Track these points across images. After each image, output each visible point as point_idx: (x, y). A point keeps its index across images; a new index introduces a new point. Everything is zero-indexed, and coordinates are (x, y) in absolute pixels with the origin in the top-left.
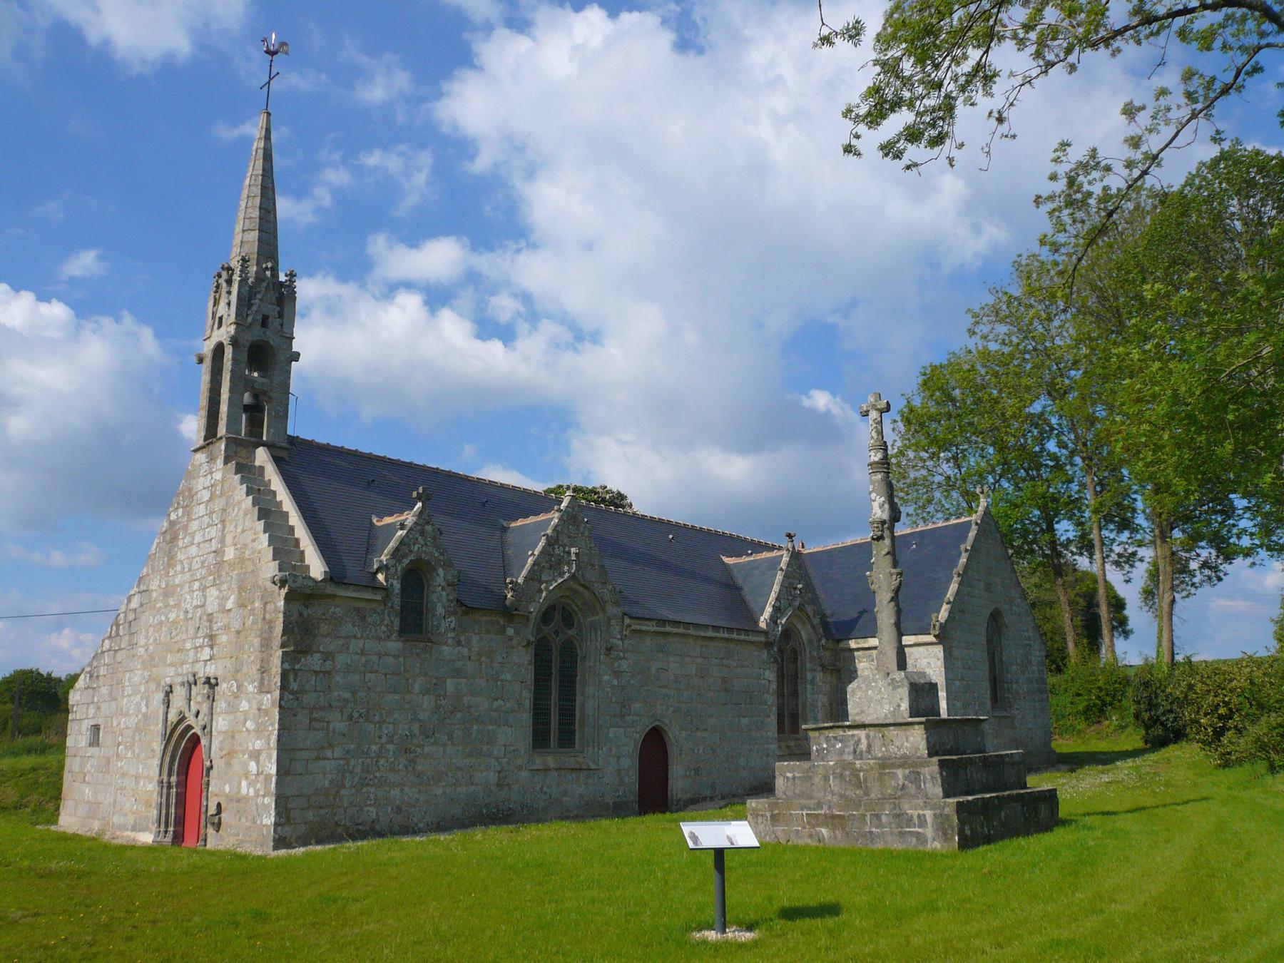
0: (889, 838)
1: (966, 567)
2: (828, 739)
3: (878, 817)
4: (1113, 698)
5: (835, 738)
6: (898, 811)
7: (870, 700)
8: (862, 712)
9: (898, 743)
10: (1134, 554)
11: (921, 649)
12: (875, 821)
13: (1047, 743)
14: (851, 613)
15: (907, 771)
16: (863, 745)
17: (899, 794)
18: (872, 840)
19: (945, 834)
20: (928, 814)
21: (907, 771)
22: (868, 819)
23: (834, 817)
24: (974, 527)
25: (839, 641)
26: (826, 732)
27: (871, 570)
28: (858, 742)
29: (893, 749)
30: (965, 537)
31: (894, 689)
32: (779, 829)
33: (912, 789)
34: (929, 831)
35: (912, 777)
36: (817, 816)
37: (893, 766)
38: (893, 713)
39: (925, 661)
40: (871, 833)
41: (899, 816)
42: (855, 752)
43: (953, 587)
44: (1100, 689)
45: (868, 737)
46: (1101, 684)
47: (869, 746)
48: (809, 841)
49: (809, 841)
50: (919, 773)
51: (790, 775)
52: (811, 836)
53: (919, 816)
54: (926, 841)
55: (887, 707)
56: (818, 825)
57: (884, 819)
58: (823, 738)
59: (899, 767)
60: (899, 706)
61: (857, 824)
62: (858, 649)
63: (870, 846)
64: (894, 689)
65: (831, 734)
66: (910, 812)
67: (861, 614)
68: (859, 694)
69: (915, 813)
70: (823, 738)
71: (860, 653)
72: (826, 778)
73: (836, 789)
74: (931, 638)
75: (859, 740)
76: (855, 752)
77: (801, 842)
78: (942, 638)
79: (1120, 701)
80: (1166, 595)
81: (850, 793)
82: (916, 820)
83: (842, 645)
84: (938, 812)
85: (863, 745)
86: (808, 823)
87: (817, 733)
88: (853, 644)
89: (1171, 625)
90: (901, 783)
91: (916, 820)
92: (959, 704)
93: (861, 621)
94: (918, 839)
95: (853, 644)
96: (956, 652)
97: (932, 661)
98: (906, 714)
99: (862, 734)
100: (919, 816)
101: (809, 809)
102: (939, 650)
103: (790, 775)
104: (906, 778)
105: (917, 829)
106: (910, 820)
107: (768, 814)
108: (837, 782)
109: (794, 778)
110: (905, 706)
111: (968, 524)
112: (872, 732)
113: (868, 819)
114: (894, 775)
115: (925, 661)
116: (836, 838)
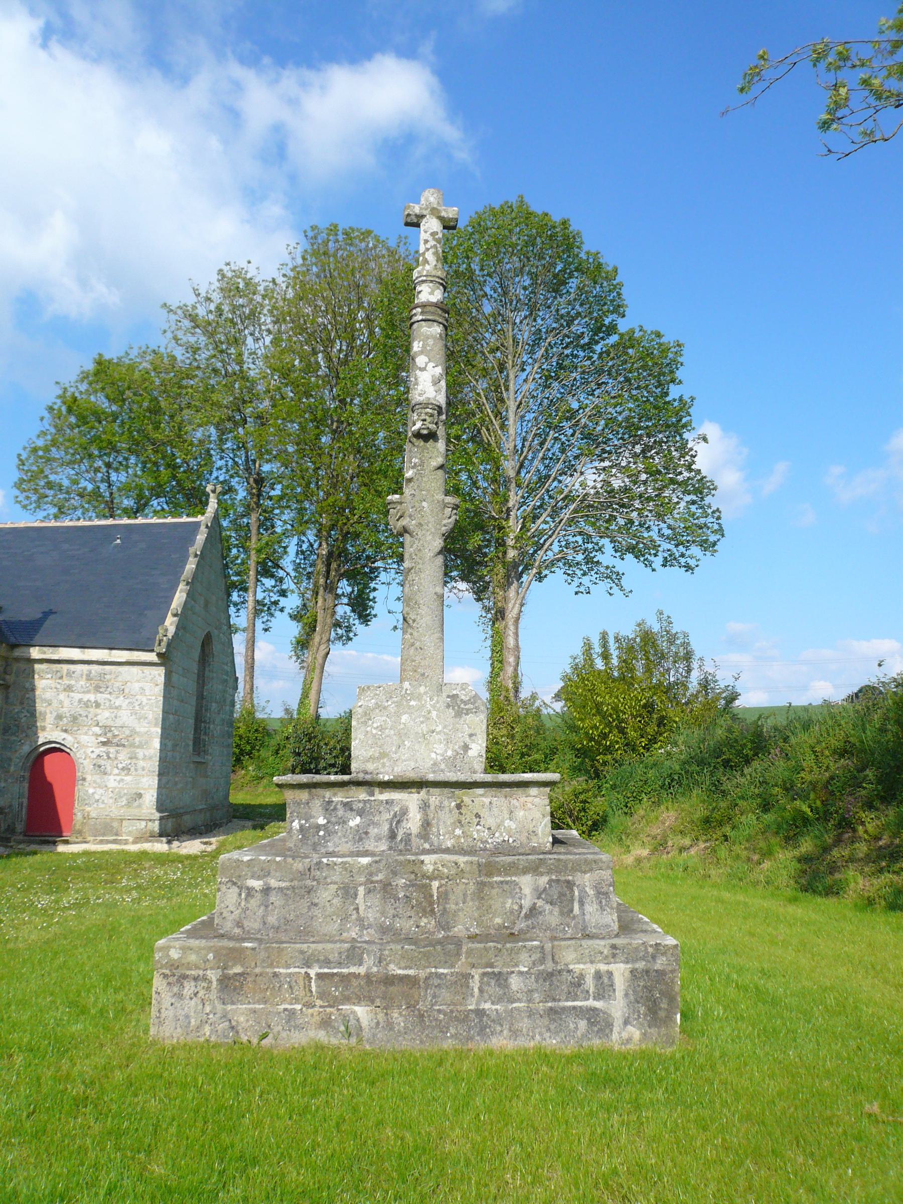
0: (524, 1024)
1: (195, 576)
2: (328, 807)
3: (501, 979)
4: (253, 748)
5: (348, 806)
6: (549, 966)
7: (402, 735)
8: (383, 755)
9: (491, 822)
10: (276, 603)
11: (135, 669)
12: (493, 989)
13: (227, 796)
14: (30, 613)
15: (543, 880)
16: (413, 822)
17: (522, 925)
18: (482, 1031)
19: (653, 1010)
20: (620, 971)
21: (543, 880)
22: (475, 984)
23: (390, 980)
24: (203, 528)
25: (14, 646)
26: (328, 794)
27: (399, 490)
28: (401, 817)
29: (477, 832)
30: (192, 541)
31: (459, 714)
32: (241, 1012)
33: (552, 916)
34: (617, 1007)
35: (555, 892)
36: (345, 979)
37: (512, 869)
38: (452, 763)
39: (137, 686)
40: (480, 1013)
41: (550, 977)
42: (393, 835)
43: (179, 598)
44: (241, 737)
45: (424, 806)
46: (241, 731)
47: (426, 824)
48: (322, 1036)
49: (322, 1036)
50: (570, 885)
51: (257, 884)
52: (326, 1023)
53: (598, 975)
54: (610, 1025)
55: (440, 748)
56: (347, 999)
57: (515, 982)
58: (317, 804)
59: (525, 871)
60: (466, 748)
61: (445, 995)
62: (41, 661)
63: (479, 1045)
64: (459, 714)
65: (339, 797)
66: (577, 968)
67: (47, 614)
68: (379, 719)
69: (590, 970)
70: (317, 804)
71: (44, 666)
72: (348, 892)
73: (371, 916)
74: (152, 657)
75: (404, 812)
76: (393, 835)
77: (299, 1038)
78: (165, 659)
79: (259, 750)
80: (323, 647)
81: (406, 925)
82: (590, 984)
83: (18, 653)
84: (641, 965)
85: (413, 822)
86: (322, 995)
87: (304, 795)
88: (35, 653)
89: (321, 678)
90: (527, 903)
91: (590, 984)
92: (170, 744)
93: (48, 624)
94: (591, 1024)
95: (35, 653)
96: (175, 677)
97: (148, 686)
98: (479, 765)
99: (411, 800)
100: (598, 975)
101: (327, 962)
102: (159, 673)
103: (257, 884)
104: (539, 893)
105: (591, 1003)
106: (578, 982)
107: (213, 975)
108: (376, 900)
109: (267, 890)
110: (478, 748)
111: (198, 524)
112: (435, 797)
113: (475, 984)
114: (512, 889)
115: (137, 686)
116: (390, 1026)
